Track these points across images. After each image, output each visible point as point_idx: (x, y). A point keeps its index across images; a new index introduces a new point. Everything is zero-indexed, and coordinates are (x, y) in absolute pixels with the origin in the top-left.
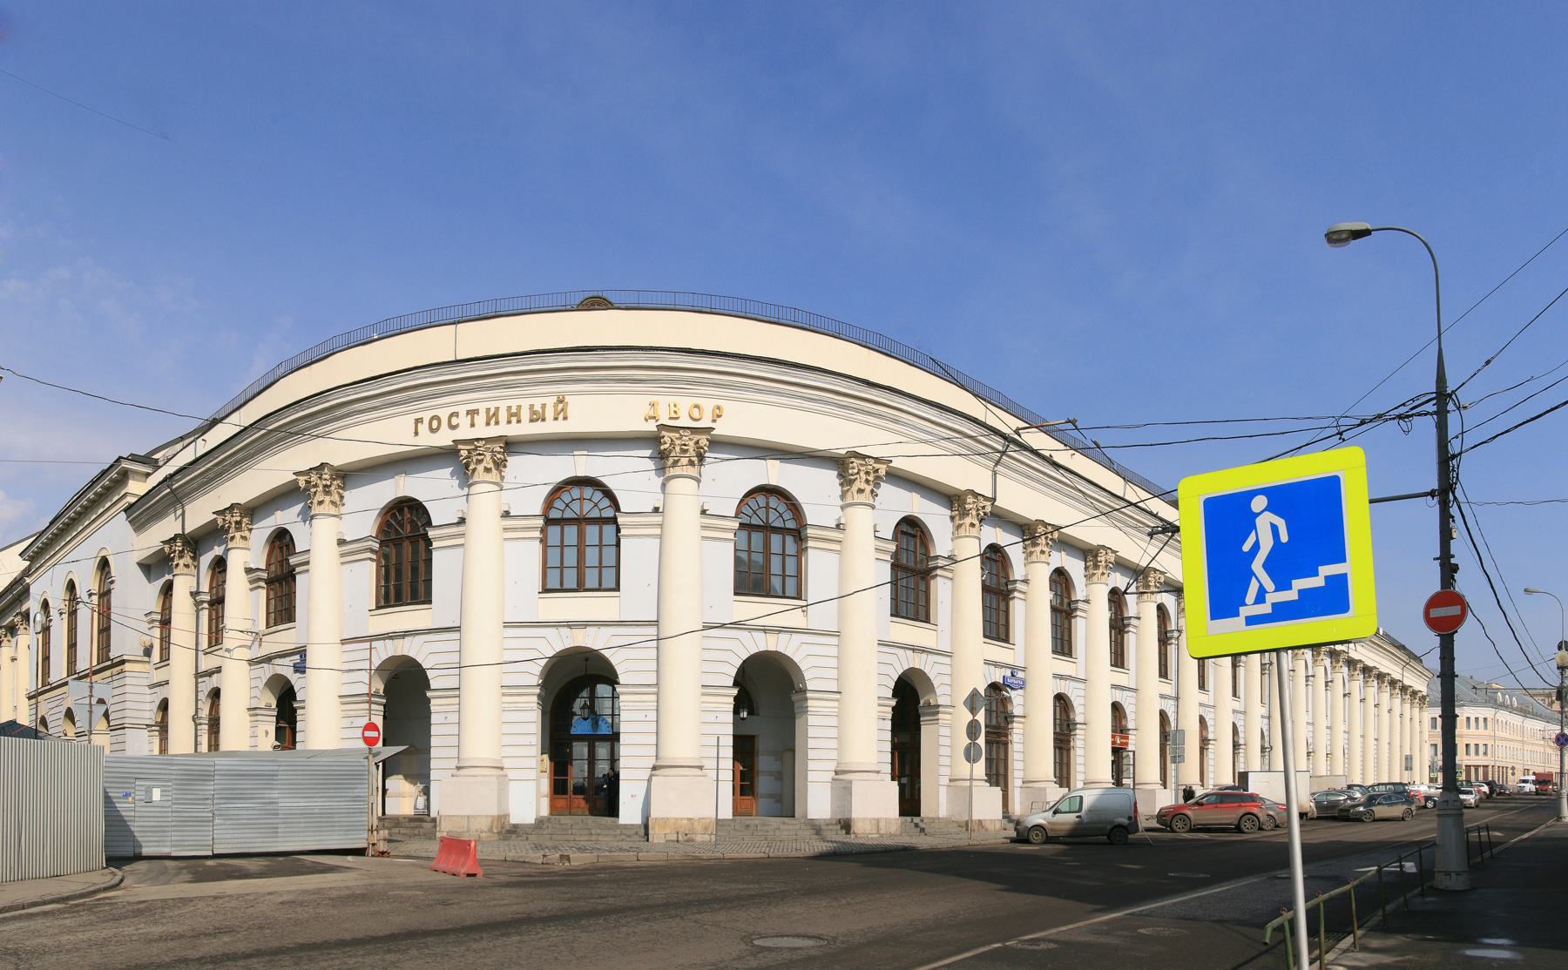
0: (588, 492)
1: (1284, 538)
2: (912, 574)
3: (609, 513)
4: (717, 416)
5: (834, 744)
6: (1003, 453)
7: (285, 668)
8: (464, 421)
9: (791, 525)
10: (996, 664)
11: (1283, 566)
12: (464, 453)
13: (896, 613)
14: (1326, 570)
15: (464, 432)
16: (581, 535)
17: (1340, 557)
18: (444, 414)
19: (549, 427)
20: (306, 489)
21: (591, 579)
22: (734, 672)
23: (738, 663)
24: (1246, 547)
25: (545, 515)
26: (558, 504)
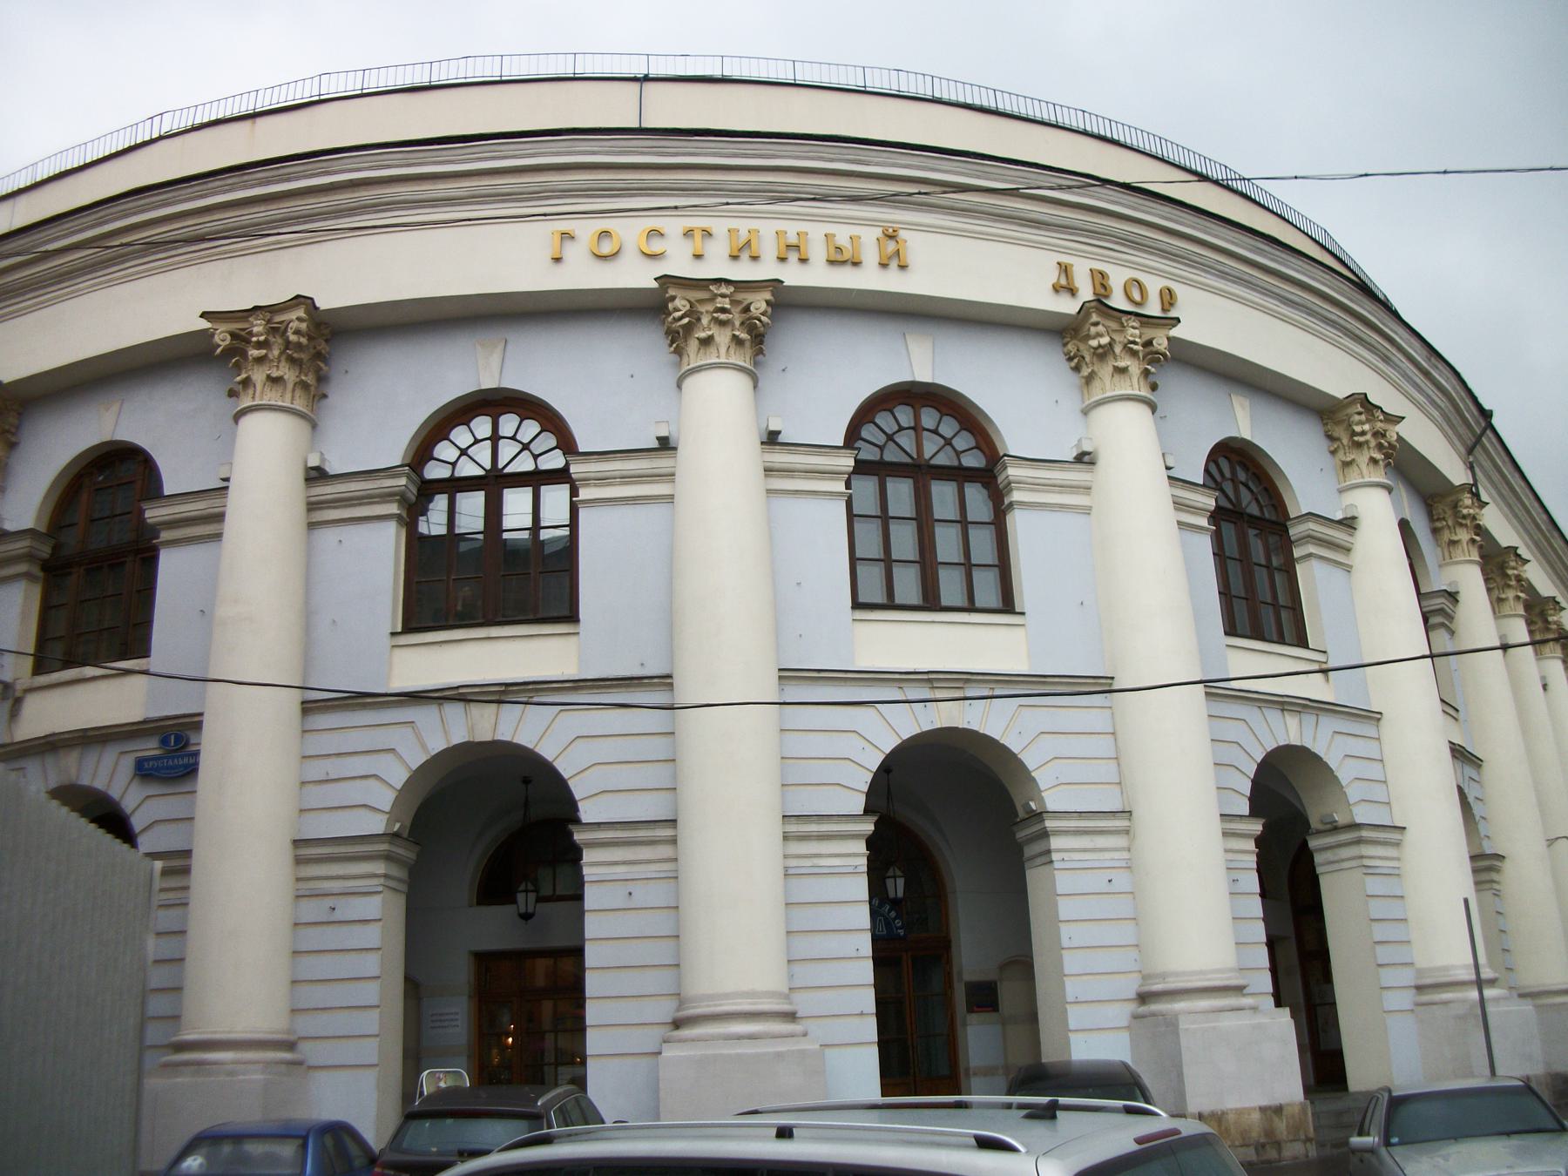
5: (1125, 933)
9: (973, 460)
12: (680, 304)
13: (1231, 630)
19: (869, 279)
20: (229, 352)
21: (950, 586)
22: (863, 781)
23: (875, 761)
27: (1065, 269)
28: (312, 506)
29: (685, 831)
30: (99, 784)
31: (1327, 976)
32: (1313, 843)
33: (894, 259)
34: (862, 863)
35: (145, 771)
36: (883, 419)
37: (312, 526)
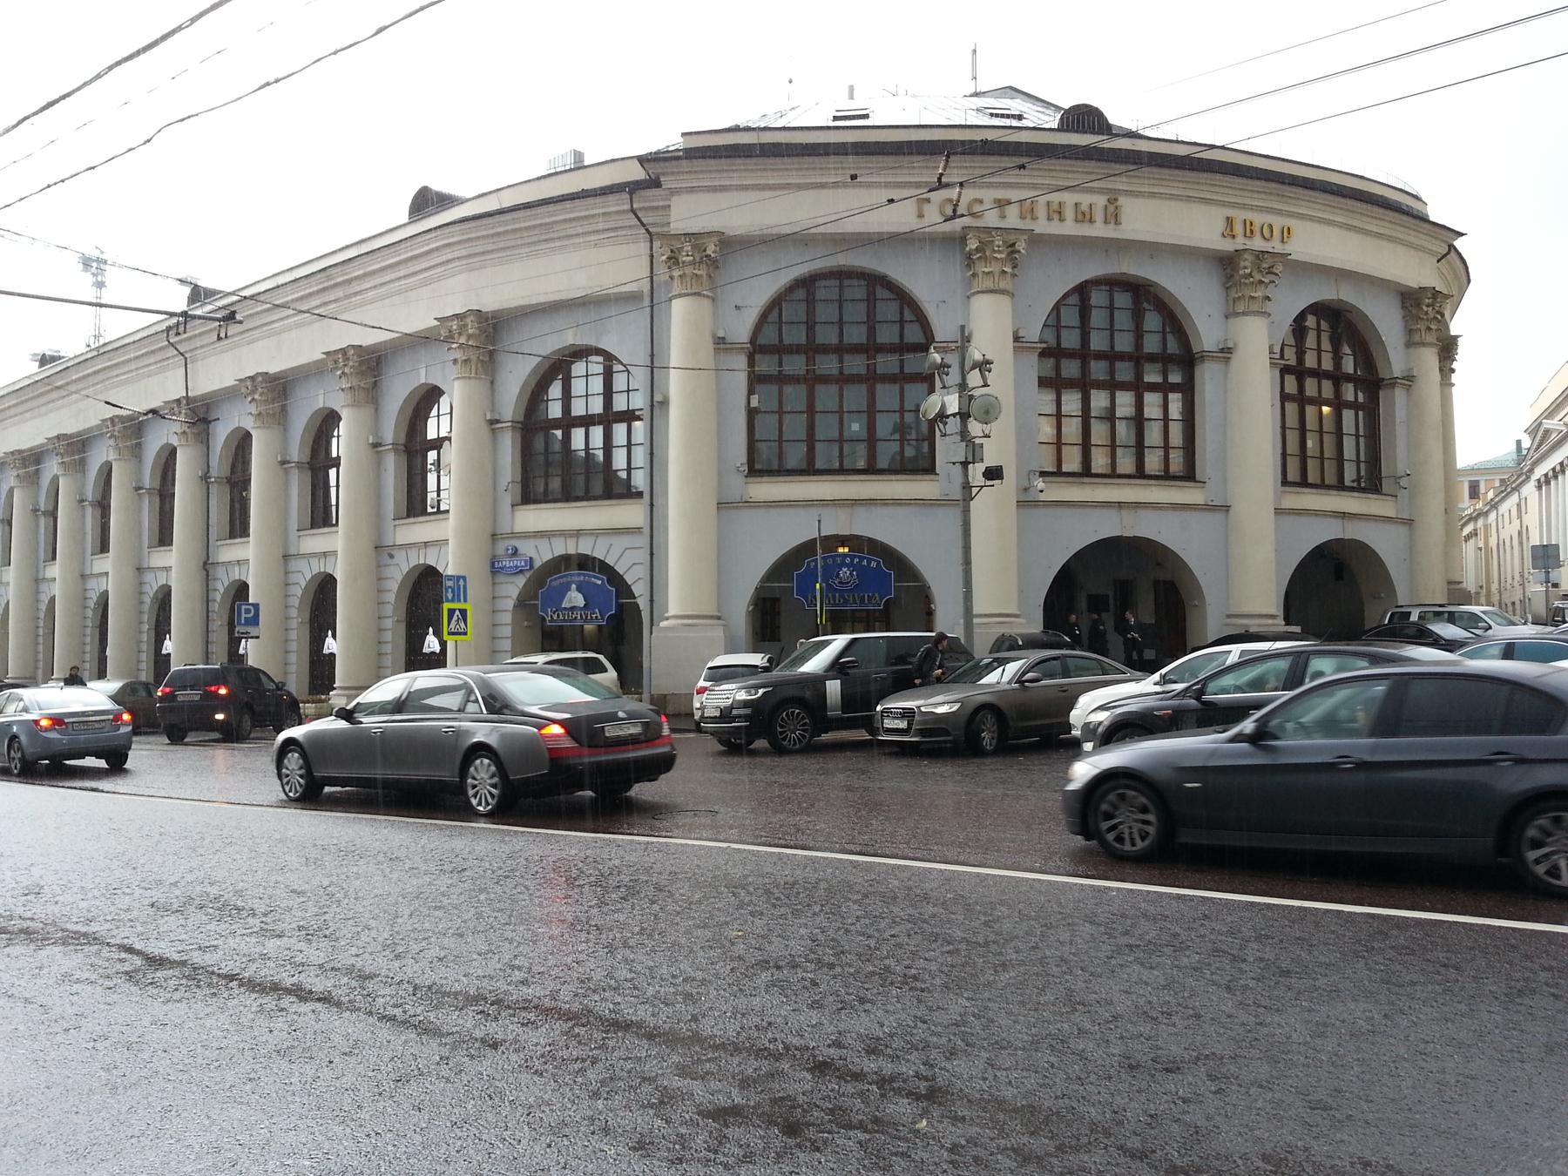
4: (1286, 233)
19: (1099, 230)
33: (1113, 217)
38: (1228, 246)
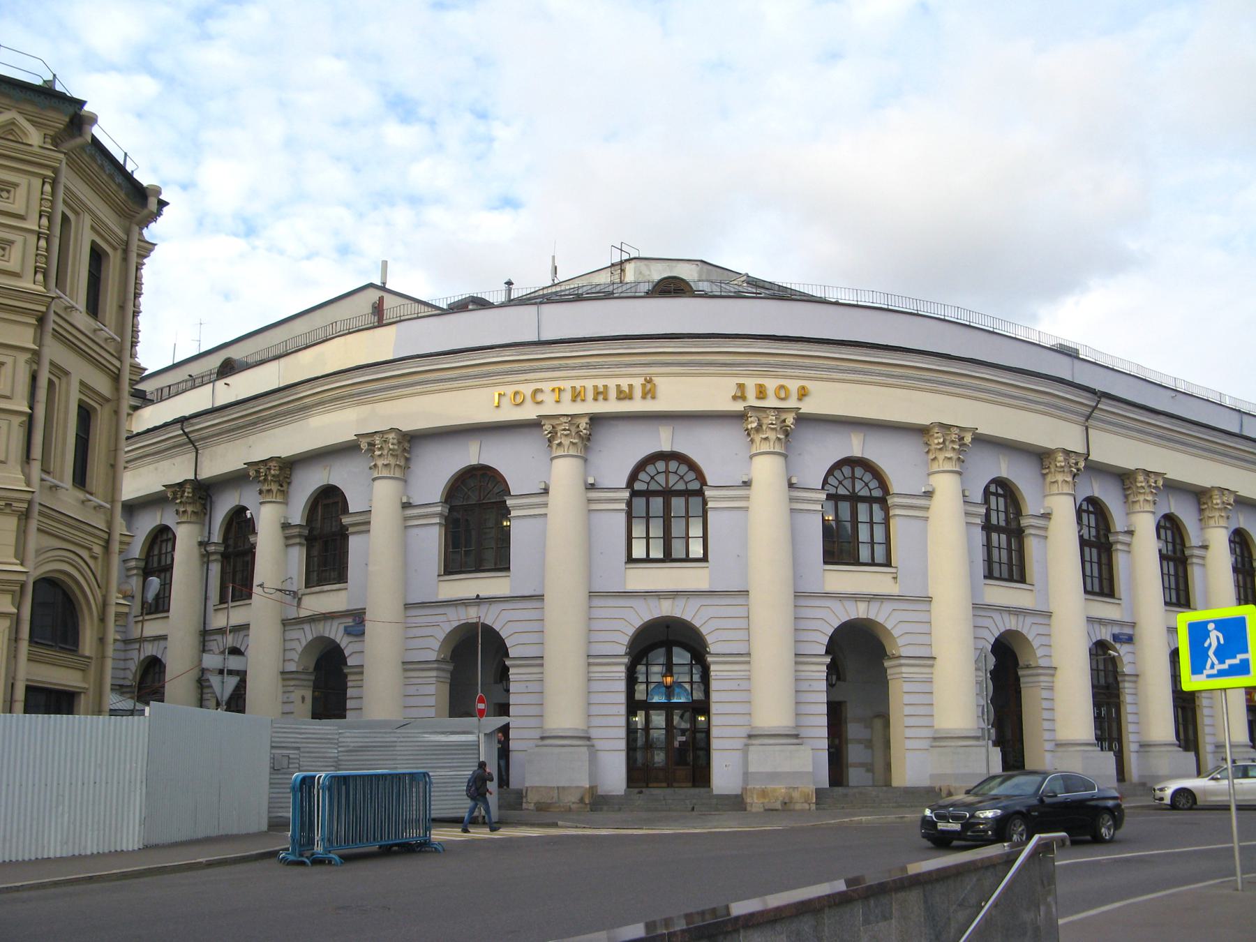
0: (673, 465)
1: (1222, 642)
2: (1004, 541)
3: (695, 486)
4: (803, 394)
6: (1095, 408)
7: (335, 632)
8: (548, 398)
9: (877, 493)
10: (1101, 622)
11: (1222, 654)
14: (1240, 657)
15: (549, 409)
16: (667, 507)
17: (1246, 651)
18: (527, 389)
19: (637, 405)
22: (826, 640)
23: (830, 631)
24: (1206, 645)
25: (630, 484)
26: (642, 476)
27: (741, 387)
28: (406, 519)
29: (546, 661)
30: (332, 636)
31: (48, 711)
32: (1020, 673)
34: (623, 675)
35: (348, 632)
36: (837, 473)
37: (406, 527)
38: (739, 406)
